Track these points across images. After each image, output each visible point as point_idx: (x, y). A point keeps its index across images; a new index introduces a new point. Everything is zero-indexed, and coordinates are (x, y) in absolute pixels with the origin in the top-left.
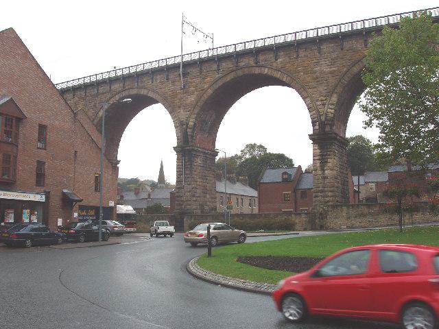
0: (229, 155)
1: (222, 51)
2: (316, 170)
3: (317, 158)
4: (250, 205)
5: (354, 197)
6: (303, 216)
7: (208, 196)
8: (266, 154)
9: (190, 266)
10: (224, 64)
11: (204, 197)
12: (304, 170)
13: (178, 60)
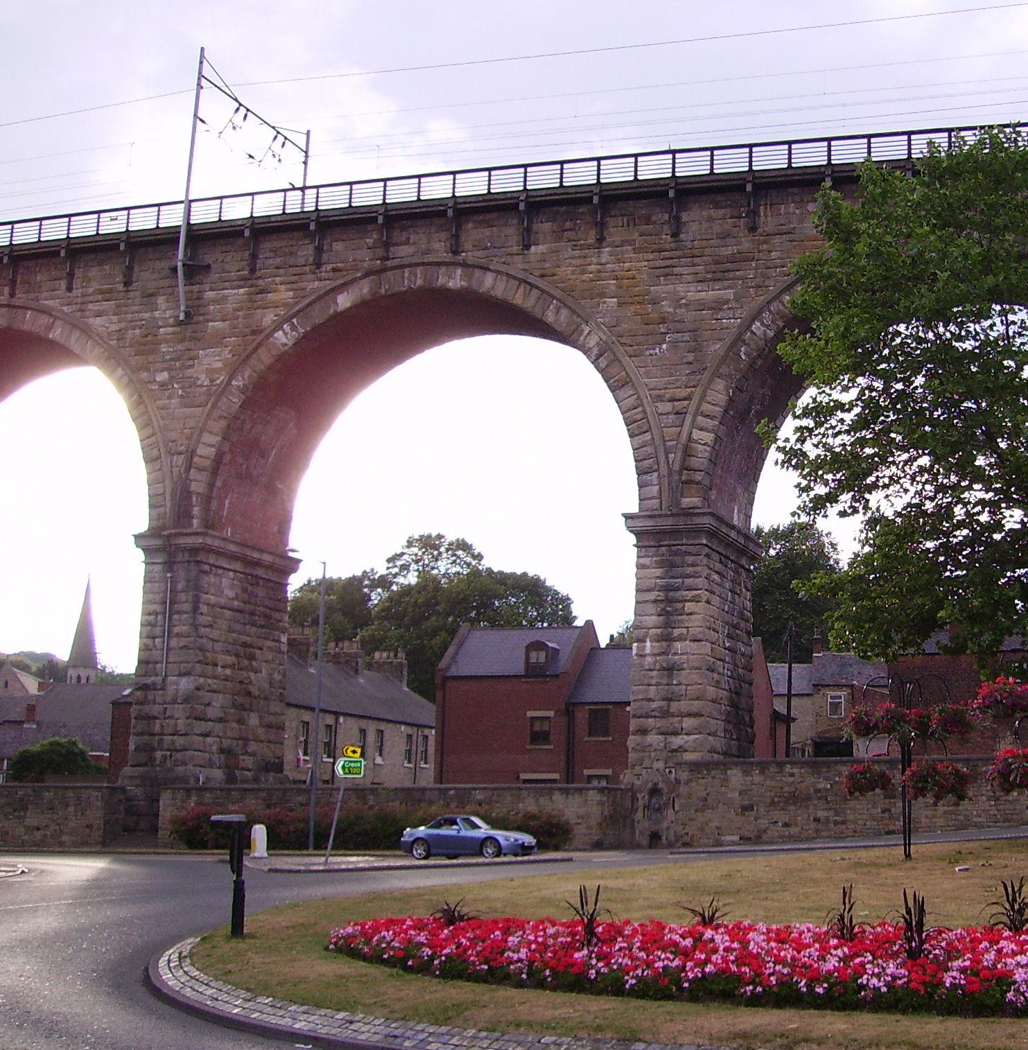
0: (342, 570)
1: (334, 200)
2: (641, 640)
3: (652, 596)
4: (409, 755)
5: (773, 735)
6: (593, 796)
7: (254, 720)
8: (475, 573)
9: (167, 976)
10: (338, 246)
11: (241, 721)
12: (604, 641)
13: (173, 218)
